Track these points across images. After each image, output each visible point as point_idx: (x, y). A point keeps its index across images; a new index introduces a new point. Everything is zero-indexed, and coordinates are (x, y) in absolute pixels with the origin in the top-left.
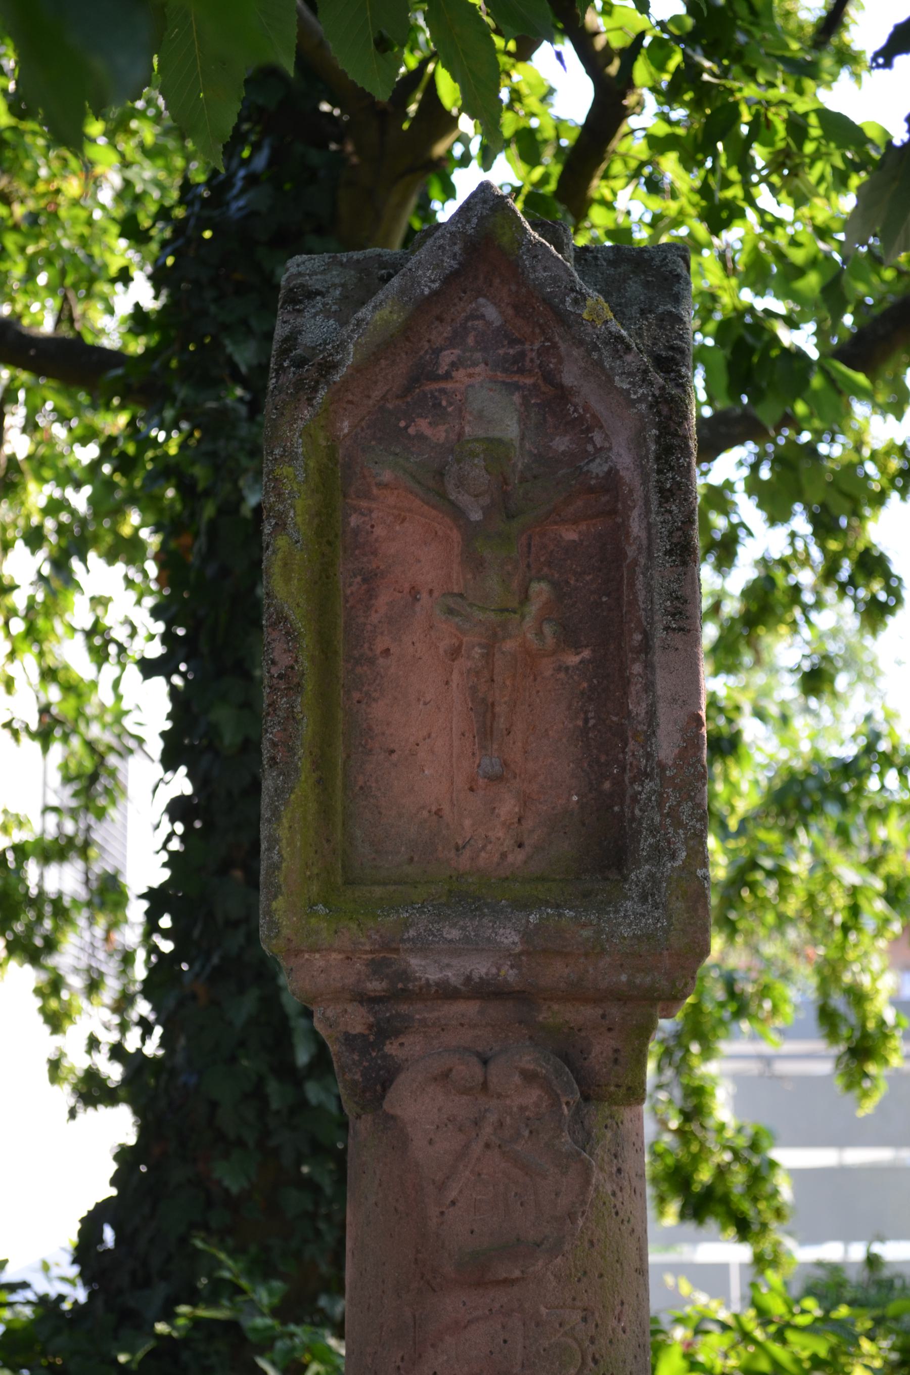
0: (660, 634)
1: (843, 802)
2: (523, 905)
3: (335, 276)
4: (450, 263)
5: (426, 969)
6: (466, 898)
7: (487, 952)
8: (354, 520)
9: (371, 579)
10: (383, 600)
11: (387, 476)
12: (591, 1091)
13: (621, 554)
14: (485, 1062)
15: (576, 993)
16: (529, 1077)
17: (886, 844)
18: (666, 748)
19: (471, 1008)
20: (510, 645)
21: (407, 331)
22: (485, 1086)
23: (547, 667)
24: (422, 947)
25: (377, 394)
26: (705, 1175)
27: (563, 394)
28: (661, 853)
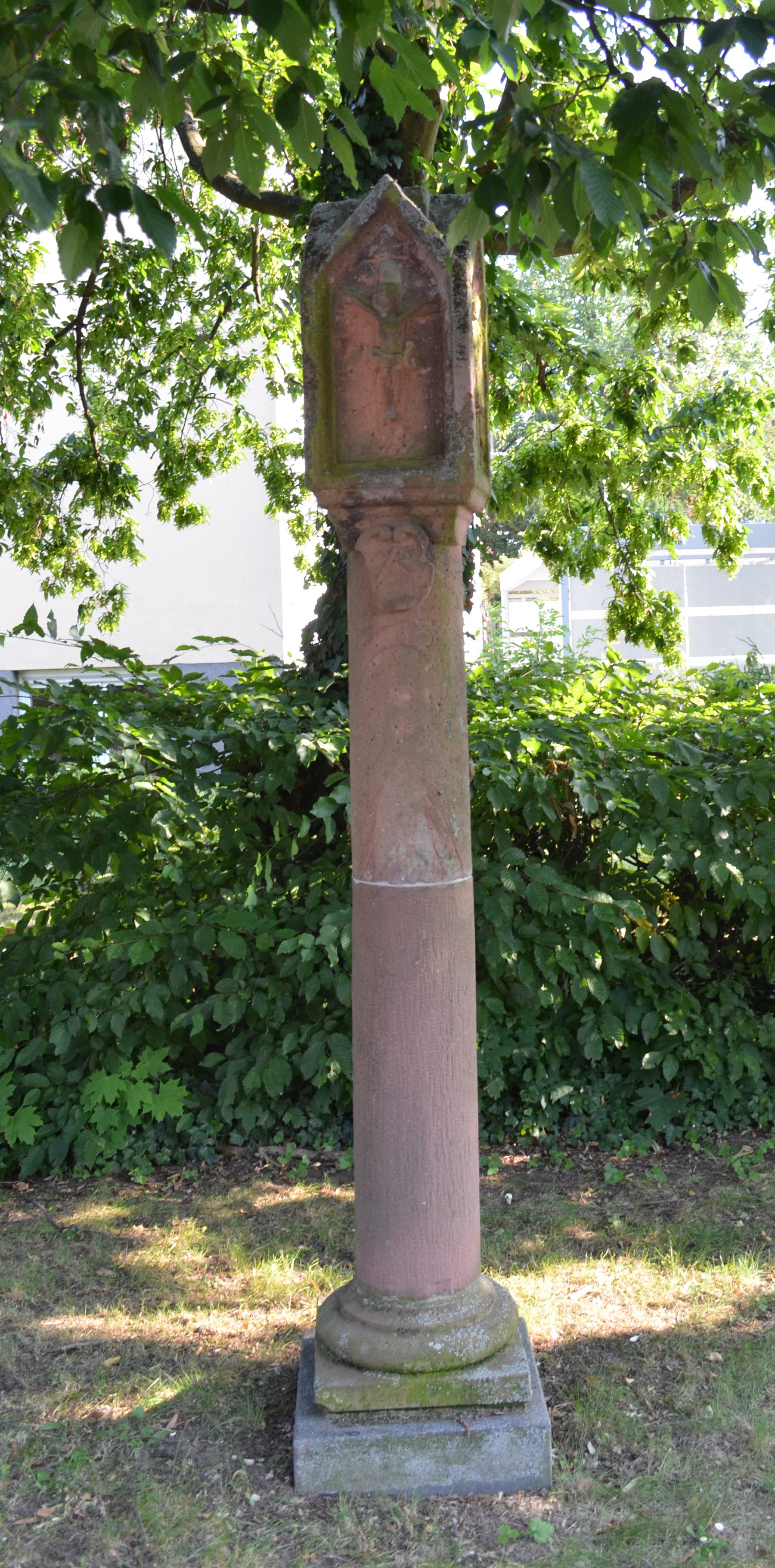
0: (455, 361)
1: (714, 419)
2: (404, 469)
3: (333, 213)
4: (371, 211)
5: (369, 495)
6: (383, 467)
7: (391, 487)
8: (337, 318)
9: (344, 341)
10: (349, 350)
11: (349, 300)
12: (433, 540)
13: (442, 328)
14: (392, 529)
15: (425, 503)
16: (409, 535)
17: (737, 441)
18: (458, 407)
19: (386, 510)
20: (398, 367)
21: (355, 239)
22: (392, 539)
23: (414, 375)
24: (366, 486)
25: (345, 265)
26: (641, 618)
27: (419, 264)
28: (456, 447)
